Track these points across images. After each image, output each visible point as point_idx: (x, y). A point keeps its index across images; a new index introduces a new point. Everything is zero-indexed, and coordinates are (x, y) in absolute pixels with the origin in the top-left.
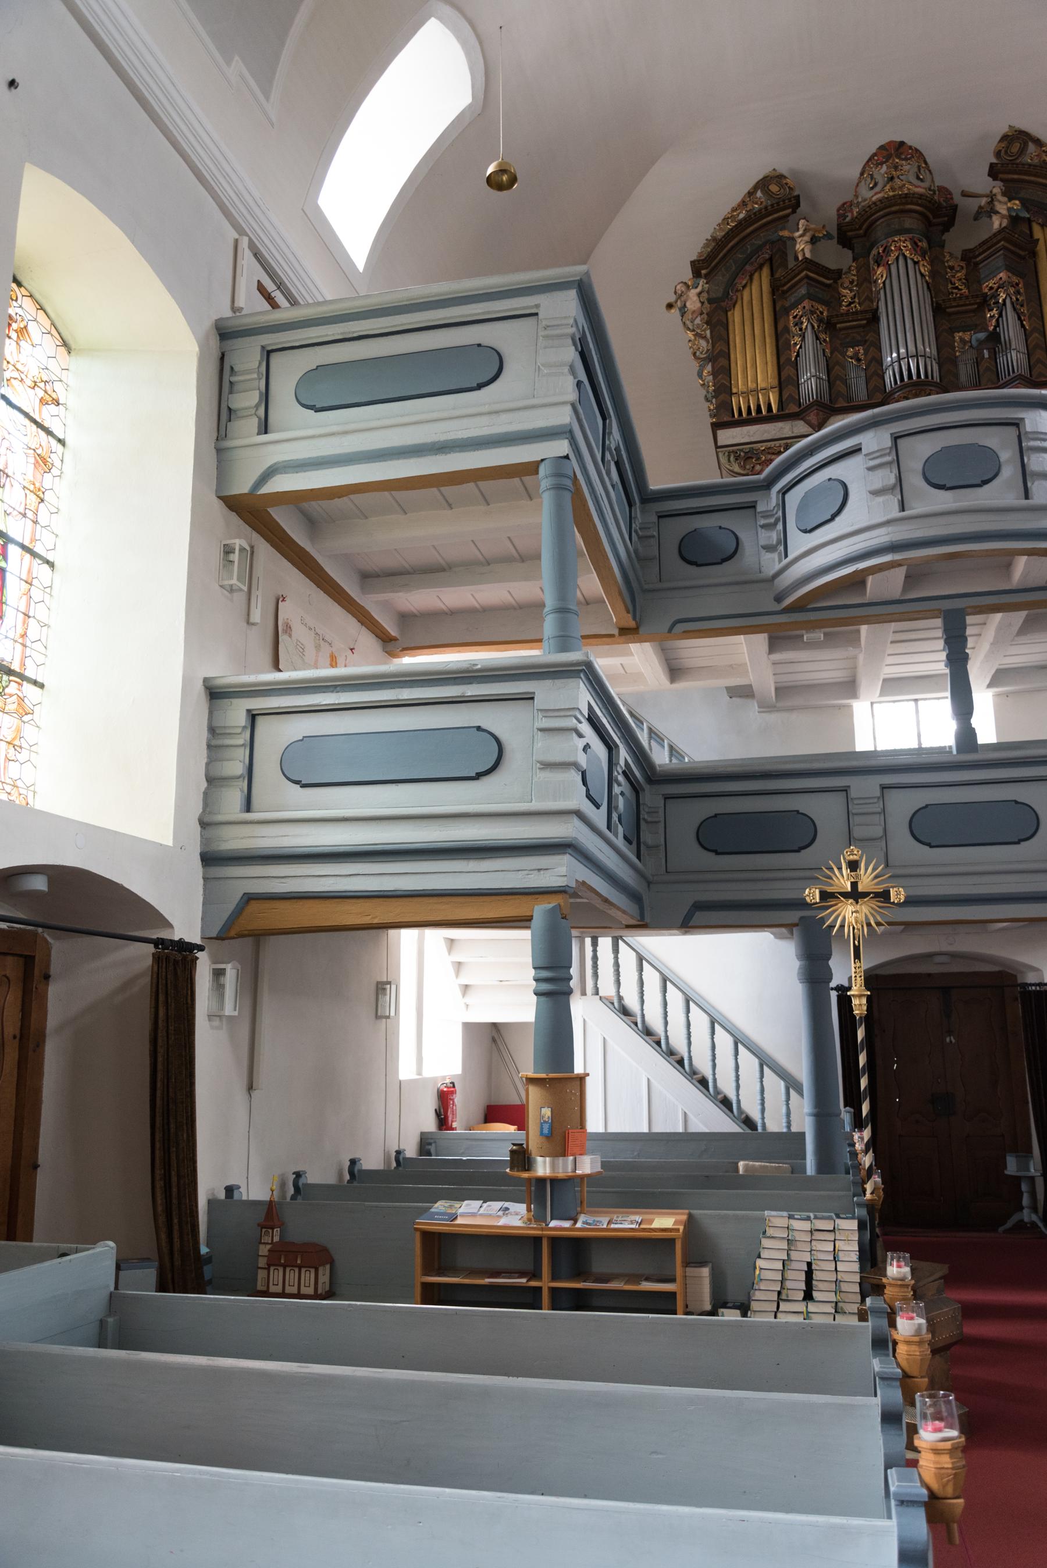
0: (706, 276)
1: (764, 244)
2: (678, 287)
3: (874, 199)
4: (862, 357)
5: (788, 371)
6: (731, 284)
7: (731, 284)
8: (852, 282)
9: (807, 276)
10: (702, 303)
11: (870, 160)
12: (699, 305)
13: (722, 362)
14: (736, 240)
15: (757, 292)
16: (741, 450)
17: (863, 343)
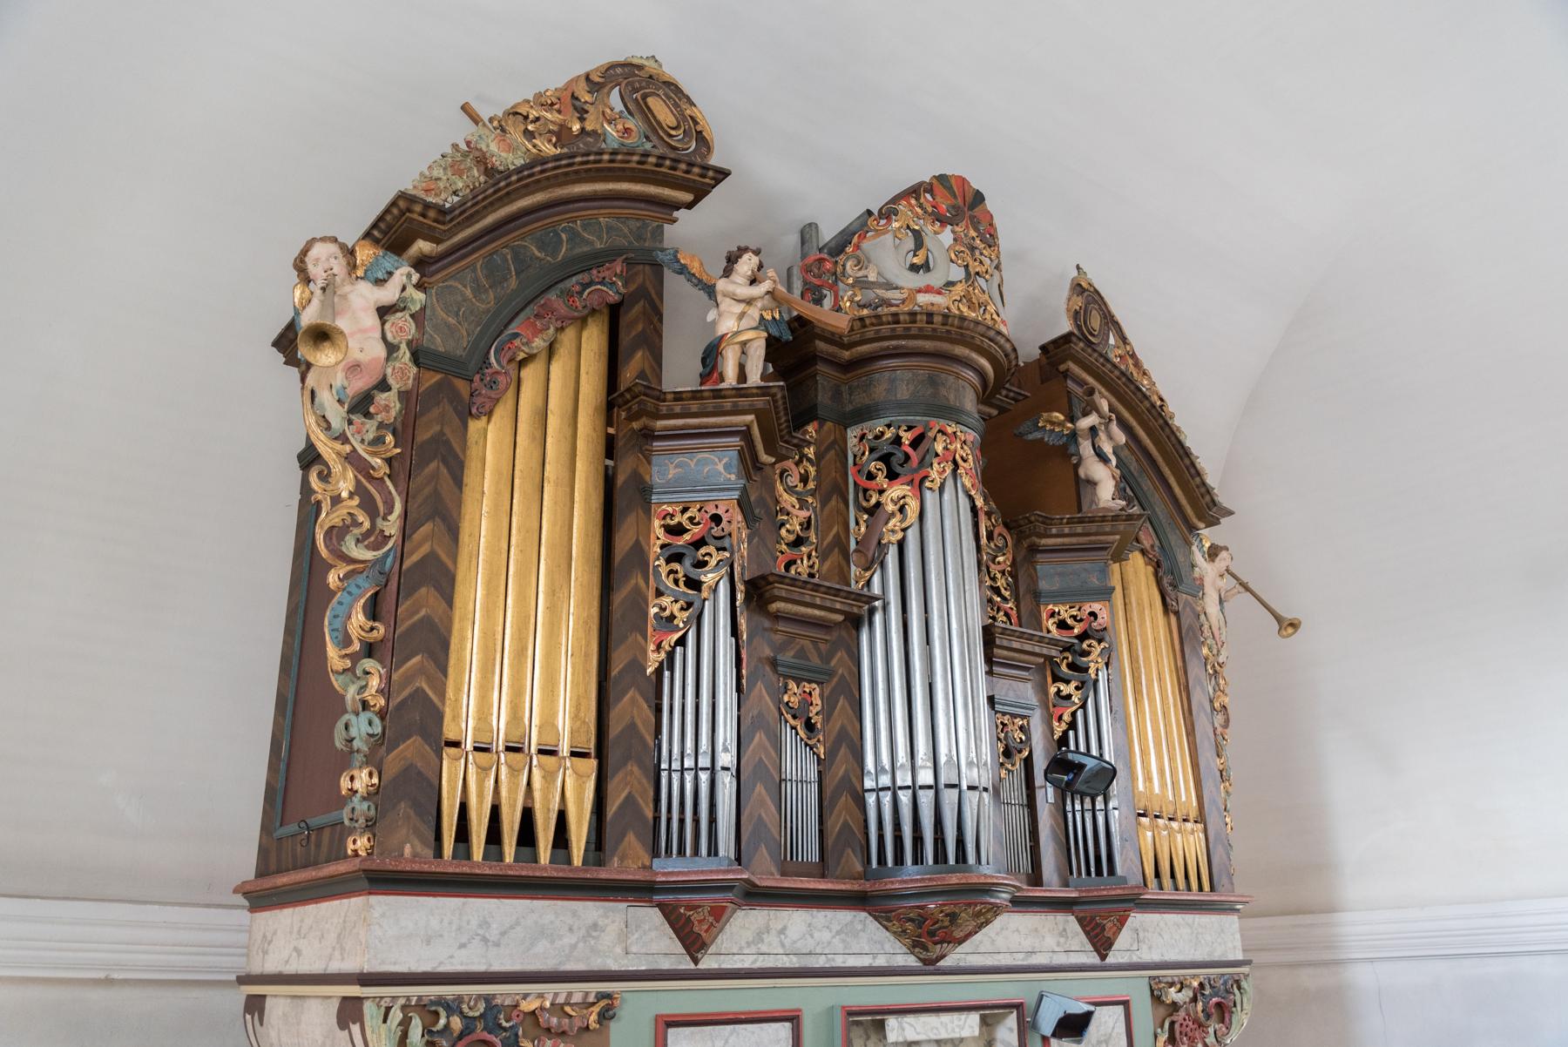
0: (420, 264)
1: (609, 255)
2: (319, 250)
3: (923, 299)
4: (817, 720)
5: (630, 708)
6: (496, 329)
7: (496, 329)
8: (804, 479)
9: (746, 434)
10: (391, 348)
11: (915, 191)
12: (380, 351)
13: (425, 601)
14: (539, 197)
15: (559, 388)
16: (452, 1007)
17: (819, 676)
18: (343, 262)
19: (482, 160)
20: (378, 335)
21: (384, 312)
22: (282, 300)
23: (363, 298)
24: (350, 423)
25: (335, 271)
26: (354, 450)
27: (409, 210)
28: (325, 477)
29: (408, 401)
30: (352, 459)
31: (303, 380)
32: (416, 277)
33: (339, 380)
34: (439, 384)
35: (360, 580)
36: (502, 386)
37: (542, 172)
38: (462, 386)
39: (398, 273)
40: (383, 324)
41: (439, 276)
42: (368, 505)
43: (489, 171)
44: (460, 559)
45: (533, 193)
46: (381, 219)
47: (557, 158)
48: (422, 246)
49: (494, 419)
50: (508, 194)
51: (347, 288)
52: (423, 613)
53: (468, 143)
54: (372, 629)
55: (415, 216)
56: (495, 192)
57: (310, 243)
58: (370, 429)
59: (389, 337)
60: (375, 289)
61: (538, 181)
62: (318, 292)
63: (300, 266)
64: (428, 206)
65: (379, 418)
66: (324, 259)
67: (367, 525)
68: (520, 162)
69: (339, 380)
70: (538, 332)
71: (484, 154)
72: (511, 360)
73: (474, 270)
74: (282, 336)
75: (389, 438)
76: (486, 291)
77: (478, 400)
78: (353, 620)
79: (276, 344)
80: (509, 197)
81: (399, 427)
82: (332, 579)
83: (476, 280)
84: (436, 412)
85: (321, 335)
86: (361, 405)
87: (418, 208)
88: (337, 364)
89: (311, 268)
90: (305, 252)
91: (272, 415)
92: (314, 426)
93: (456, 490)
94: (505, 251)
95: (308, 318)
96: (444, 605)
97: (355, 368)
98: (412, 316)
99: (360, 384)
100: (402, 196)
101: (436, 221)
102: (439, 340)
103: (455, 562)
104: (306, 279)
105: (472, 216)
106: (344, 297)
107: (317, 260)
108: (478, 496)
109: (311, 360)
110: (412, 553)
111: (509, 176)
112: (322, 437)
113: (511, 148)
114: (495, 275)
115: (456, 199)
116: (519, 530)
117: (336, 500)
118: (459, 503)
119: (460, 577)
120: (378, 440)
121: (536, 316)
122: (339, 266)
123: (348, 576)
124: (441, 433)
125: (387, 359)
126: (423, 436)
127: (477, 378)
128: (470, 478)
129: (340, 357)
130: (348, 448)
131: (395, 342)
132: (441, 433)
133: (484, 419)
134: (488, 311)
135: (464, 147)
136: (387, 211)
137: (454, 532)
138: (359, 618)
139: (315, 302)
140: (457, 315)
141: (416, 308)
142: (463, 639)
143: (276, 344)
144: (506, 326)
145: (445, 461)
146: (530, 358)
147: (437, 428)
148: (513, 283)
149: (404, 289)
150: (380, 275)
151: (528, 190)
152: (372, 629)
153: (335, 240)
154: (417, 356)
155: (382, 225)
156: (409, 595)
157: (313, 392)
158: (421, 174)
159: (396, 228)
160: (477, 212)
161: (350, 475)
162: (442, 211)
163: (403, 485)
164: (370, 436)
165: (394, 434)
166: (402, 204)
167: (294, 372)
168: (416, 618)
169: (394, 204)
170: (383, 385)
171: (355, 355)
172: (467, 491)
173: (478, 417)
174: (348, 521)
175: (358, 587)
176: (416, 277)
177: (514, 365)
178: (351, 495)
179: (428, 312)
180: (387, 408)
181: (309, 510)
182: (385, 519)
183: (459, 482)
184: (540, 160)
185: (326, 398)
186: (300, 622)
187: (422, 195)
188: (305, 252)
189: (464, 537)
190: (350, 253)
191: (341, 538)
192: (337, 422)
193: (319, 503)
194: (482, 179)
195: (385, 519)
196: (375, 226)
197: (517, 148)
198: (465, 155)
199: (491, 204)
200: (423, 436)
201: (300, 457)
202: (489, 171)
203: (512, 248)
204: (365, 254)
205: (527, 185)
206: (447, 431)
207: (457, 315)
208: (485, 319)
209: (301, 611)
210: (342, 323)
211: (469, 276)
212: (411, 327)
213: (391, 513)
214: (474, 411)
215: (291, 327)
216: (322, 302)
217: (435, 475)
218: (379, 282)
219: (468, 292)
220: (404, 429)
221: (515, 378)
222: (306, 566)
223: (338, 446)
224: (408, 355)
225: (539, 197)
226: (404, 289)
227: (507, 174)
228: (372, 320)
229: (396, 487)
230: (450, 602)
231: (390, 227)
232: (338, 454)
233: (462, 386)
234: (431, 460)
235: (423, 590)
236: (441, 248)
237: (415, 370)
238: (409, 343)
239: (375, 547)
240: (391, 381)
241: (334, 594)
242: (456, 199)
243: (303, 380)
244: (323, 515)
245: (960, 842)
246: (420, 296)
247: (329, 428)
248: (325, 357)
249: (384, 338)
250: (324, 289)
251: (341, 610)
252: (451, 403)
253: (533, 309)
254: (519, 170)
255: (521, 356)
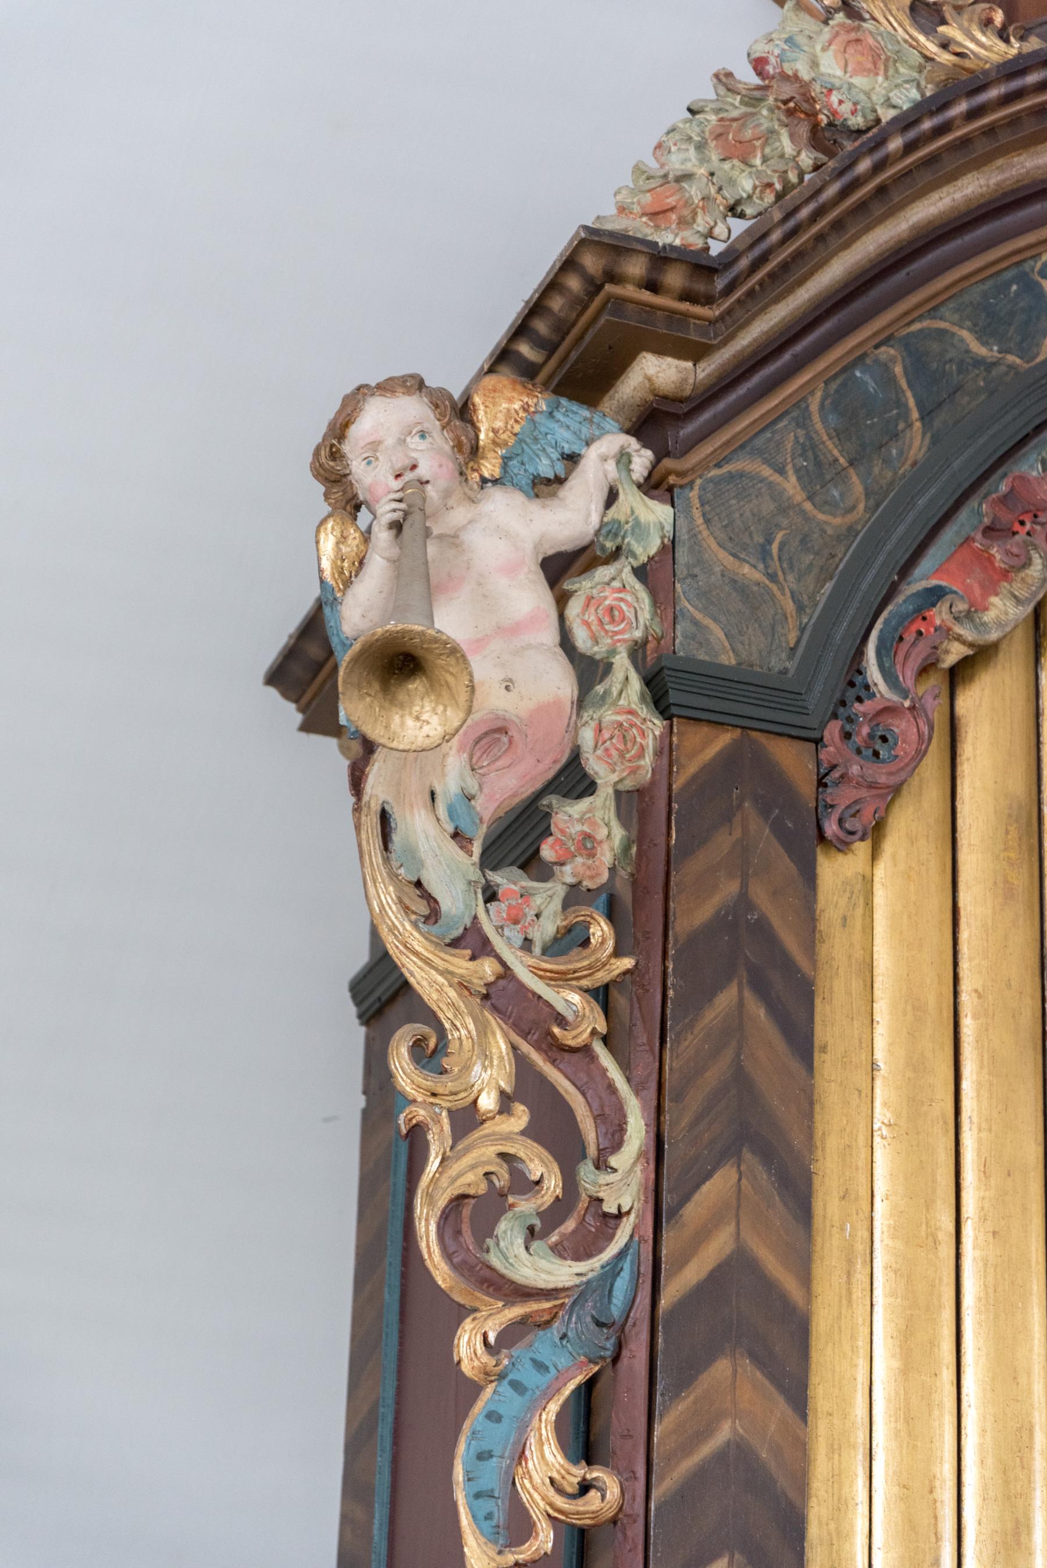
0: (652, 421)
2: (378, 419)
6: (876, 585)
10: (589, 672)
12: (558, 682)
13: (729, 1396)
18: (441, 441)
19: (801, 108)
20: (550, 636)
21: (560, 568)
22: (288, 559)
23: (505, 533)
24: (491, 896)
25: (424, 470)
26: (506, 973)
27: (612, 277)
28: (430, 1056)
29: (643, 816)
30: (502, 998)
31: (357, 783)
32: (642, 460)
33: (453, 775)
34: (729, 760)
35: (544, 1345)
36: (905, 748)
37: (972, 114)
38: (792, 760)
39: (592, 456)
40: (562, 600)
41: (706, 449)
42: (554, 1129)
43: (825, 136)
44: (819, 1270)
45: (952, 177)
46: (536, 309)
47: (1013, 69)
48: (655, 372)
49: (889, 846)
50: (882, 190)
51: (459, 515)
52: (724, 1433)
53: (759, 64)
54: (585, 1488)
55: (630, 291)
56: (844, 193)
57: (353, 402)
58: (545, 906)
59: (582, 639)
60: (534, 507)
61: (965, 142)
62: (382, 536)
63: (331, 470)
64: (661, 258)
65: (567, 874)
66: (393, 439)
67: (553, 1185)
68: (907, 97)
69: (453, 775)
70: (998, 578)
71: (805, 87)
72: (924, 670)
73: (803, 421)
74: (291, 654)
75: (601, 930)
76: (840, 476)
77: (842, 797)
78: (532, 1462)
79: (276, 677)
80: (885, 199)
81: (626, 894)
82: (468, 1348)
83: (809, 448)
84: (724, 841)
85: (400, 663)
86: (516, 841)
87: (636, 267)
88: (447, 738)
89: (357, 467)
90: (339, 429)
91: (279, 883)
92: (394, 914)
93: (795, 1065)
94: (886, 352)
95: (360, 616)
96: (782, 1407)
97: (494, 737)
98: (640, 573)
99: (510, 783)
100: (592, 239)
101: (686, 296)
102: (717, 632)
103: (806, 1279)
104: (349, 504)
105: (785, 267)
106: (453, 540)
107: (375, 445)
108: (860, 1078)
109: (375, 733)
110: (682, 1261)
111: (881, 142)
112: (417, 942)
113: (881, 61)
114: (864, 426)
115: (739, 227)
116: (985, 1172)
117: (466, 1120)
118: (807, 1104)
119: (821, 1323)
120: (572, 939)
121: (990, 531)
122: (433, 458)
123: (511, 1335)
124: (744, 901)
125: (580, 704)
126: (692, 915)
127: (833, 731)
128: (831, 1024)
129: (455, 717)
130: (488, 968)
131: (598, 651)
132: (744, 901)
133: (862, 848)
134: (851, 531)
135: (748, 76)
136: (552, 286)
137: (796, 1191)
138: (546, 1459)
139: (377, 566)
140: (764, 554)
141: (646, 548)
142: (841, 1507)
143: (276, 677)
144: (905, 570)
145: (761, 987)
146: (980, 656)
147: (730, 889)
148: (916, 442)
149: (612, 497)
150: (545, 468)
151: (934, 171)
152: (585, 1488)
153: (416, 384)
154: (658, 689)
155: (541, 326)
156: (684, 1381)
157: (384, 817)
158: (639, 170)
159: (577, 332)
160: (799, 255)
161: (500, 1044)
162: (702, 267)
163: (645, 1064)
164: (547, 928)
165: (611, 915)
166: (591, 262)
167: (328, 756)
168: (707, 1450)
169: (569, 264)
170: (573, 780)
171: (494, 701)
172: (827, 1065)
173: (842, 846)
174: (502, 1179)
175: (540, 1366)
176: (642, 460)
177: (935, 682)
178: (506, 1103)
179: (683, 556)
180: (587, 844)
181: (391, 1155)
182: (601, 1165)
183: (802, 1043)
184: (964, 83)
185: (421, 830)
186: (383, 1461)
187: (641, 228)
188: (339, 429)
189: (828, 1204)
190: (463, 411)
191: (485, 1230)
192: (455, 898)
193: (416, 1135)
194: (806, 159)
195: (601, 1165)
196: (521, 330)
197: (899, 57)
198: (753, 99)
199: (838, 225)
200: (692, 915)
201: (359, 989)
202: (825, 136)
203: (908, 345)
204: (501, 410)
205: (932, 160)
206: (760, 895)
207: (764, 554)
208: (845, 557)
209: (385, 1430)
210: (451, 621)
211: (790, 438)
212: (638, 609)
213: (617, 1145)
214: (831, 828)
215: (314, 627)
216: (396, 563)
217: (735, 1027)
218: (545, 487)
219: (791, 486)
220: (637, 902)
221: (939, 718)
222: (391, 1297)
223: (460, 964)
224: (636, 684)
225: (970, 188)
226: (612, 497)
227: (873, 135)
228: (530, 597)
229: (625, 1067)
230: (797, 1395)
231: (562, 329)
232: (463, 986)
233: (792, 760)
234: (718, 987)
235: (722, 1368)
236: (707, 369)
237: (657, 725)
238: (637, 651)
239: (580, 1248)
240: (594, 764)
241: (474, 1389)
242: (739, 227)
243: (357, 783)
244: (433, 1164)
245: (555, 973)
246: (657, 514)
247: (433, 914)
248: (417, 722)
249: (566, 643)
250: (397, 527)
251: (497, 1437)
252: (765, 811)
253: (981, 509)
254: (906, 121)
255: (955, 653)
